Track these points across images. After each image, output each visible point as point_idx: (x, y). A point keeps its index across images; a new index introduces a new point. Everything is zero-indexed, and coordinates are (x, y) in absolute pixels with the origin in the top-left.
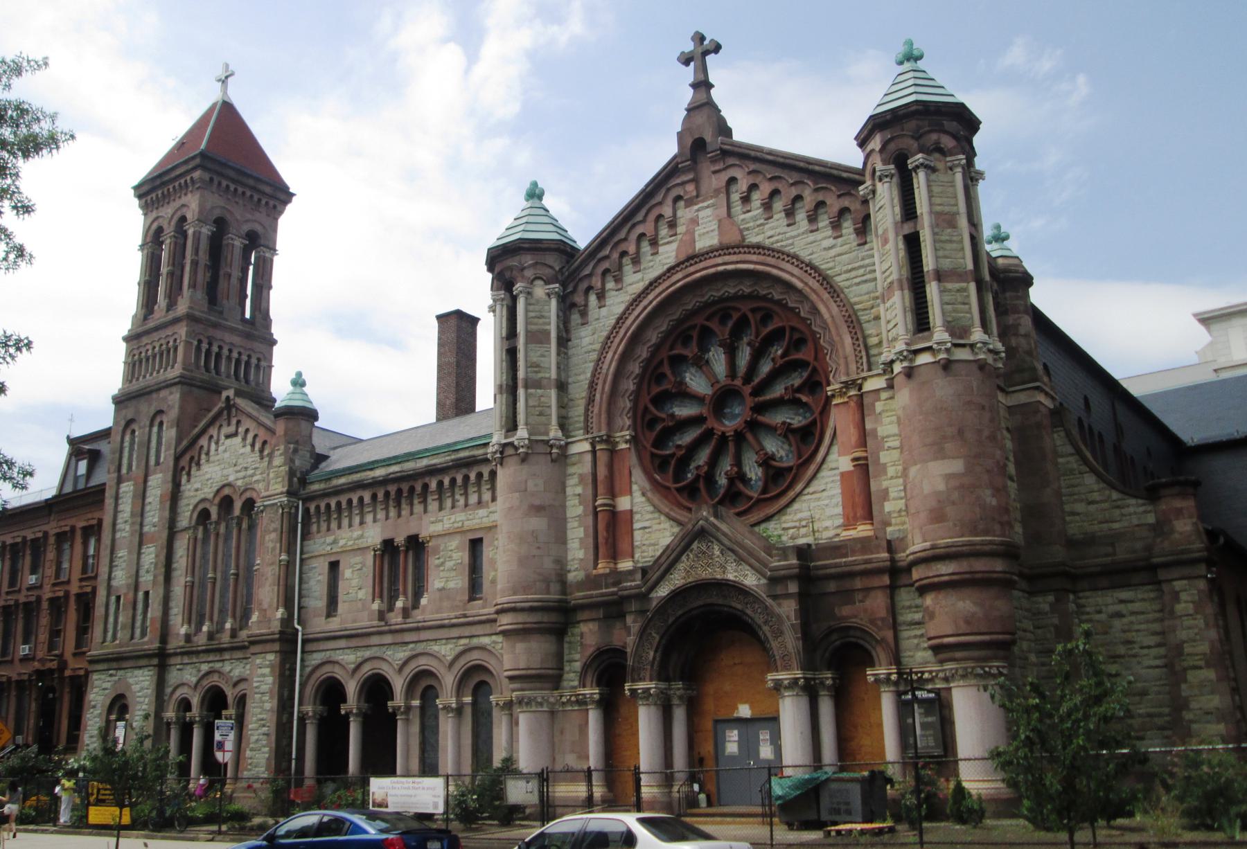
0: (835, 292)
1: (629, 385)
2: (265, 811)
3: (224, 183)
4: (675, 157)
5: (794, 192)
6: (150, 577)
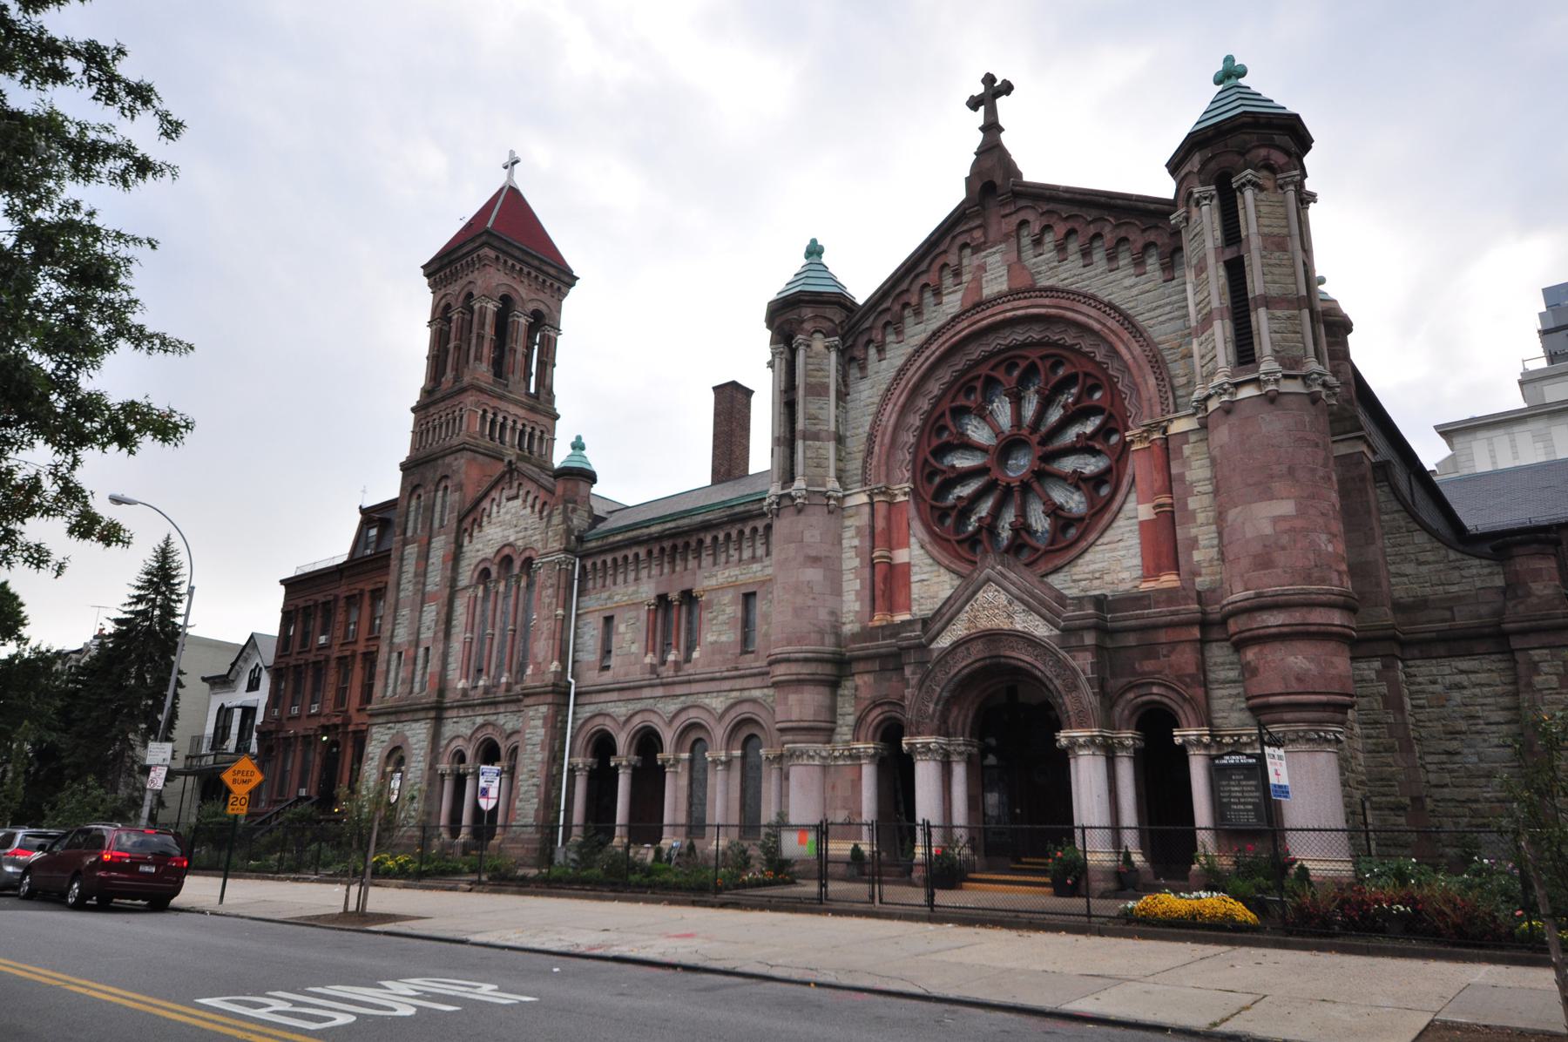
0: (1136, 331)
1: (909, 438)
2: (531, 861)
3: (510, 262)
4: (963, 203)
5: (1092, 230)
6: (430, 634)
